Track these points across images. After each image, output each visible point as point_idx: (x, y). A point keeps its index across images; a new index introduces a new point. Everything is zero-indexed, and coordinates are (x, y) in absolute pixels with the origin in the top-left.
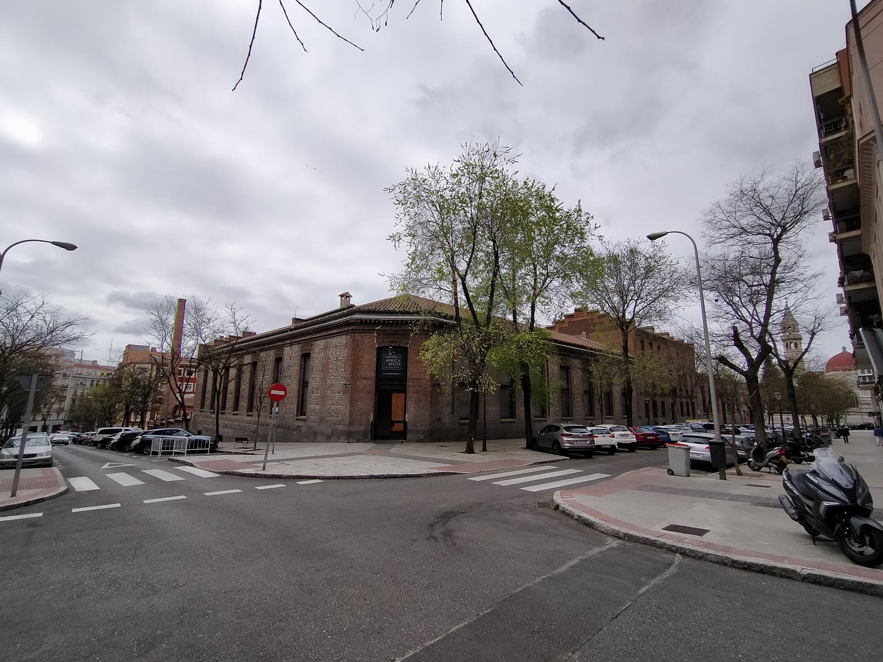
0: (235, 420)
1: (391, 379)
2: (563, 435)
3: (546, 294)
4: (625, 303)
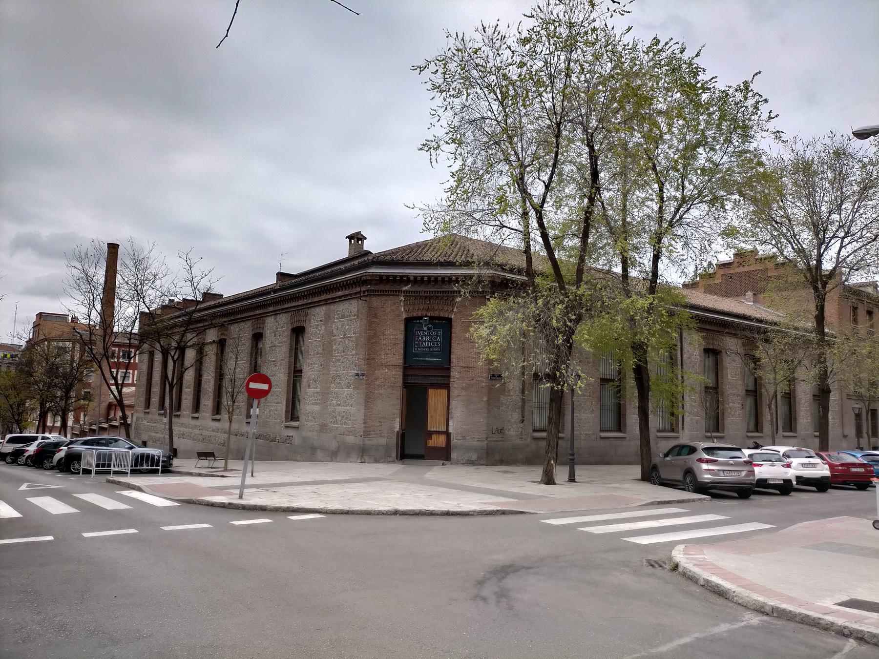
0: (195, 427)
1: (429, 367)
2: (700, 460)
3: (680, 232)
4: (822, 244)
